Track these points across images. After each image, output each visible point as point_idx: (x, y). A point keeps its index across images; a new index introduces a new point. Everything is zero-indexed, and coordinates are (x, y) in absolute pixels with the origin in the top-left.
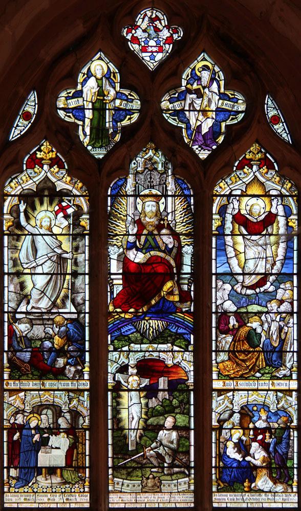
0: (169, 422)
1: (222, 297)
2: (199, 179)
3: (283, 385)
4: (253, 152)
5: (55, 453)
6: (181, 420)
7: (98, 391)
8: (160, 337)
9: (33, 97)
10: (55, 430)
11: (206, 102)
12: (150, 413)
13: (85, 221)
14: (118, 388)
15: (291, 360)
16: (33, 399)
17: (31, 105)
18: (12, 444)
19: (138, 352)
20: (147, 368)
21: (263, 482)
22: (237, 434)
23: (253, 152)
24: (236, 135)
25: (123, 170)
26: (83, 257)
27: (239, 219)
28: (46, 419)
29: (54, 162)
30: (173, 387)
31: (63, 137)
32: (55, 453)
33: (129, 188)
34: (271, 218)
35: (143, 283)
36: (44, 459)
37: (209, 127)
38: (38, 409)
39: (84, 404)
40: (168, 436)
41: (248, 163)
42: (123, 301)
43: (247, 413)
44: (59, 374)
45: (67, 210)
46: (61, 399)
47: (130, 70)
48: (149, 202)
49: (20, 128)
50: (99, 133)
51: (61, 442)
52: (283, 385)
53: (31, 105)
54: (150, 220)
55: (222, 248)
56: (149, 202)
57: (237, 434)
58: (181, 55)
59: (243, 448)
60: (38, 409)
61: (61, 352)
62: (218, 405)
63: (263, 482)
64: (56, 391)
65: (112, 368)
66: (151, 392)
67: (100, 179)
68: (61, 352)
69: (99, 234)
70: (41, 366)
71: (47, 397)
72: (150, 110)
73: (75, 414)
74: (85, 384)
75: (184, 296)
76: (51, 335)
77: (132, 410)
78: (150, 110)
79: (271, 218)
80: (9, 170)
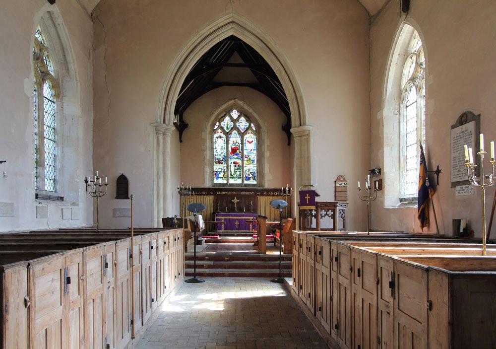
0: (238, 171)
1: (245, 153)
2: (242, 135)
3: (254, 166)
4: (250, 131)
5: (221, 175)
6: (240, 171)
7: (227, 166)
8: (237, 158)
9: (218, 123)
10: (221, 172)
11: (243, 124)
12: (235, 169)
13: (226, 141)
14: (230, 166)
15: (256, 162)
16: (218, 167)
17: (218, 124)
18: (216, 174)
19: (233, 161)
20: (234, 163)
21: (252, 180)
22: (248, 173)
23: (250, 131)
24: (247, 129)
25: (231, 134)
26: (225, 147)
27: (248, 141)
28: (220, 170)
29: (221, 132)
30: (238, 166)
31: (222, 128)
32: (221, 175)
33: (232, 137)
34: (252, 141)
35: (234, 151)
36: (220, 176)
37: (436, 194)
38: (219, 169)
39: (226, 168)
40: (238, 173)
41: (249, 133)
42: (231, 153)
43: (249, 170)
44: (222, 163)
45: (235, 119)
46: (223, 168)
47: (232, 119)
48: (235, 138)
49: (216, 127)
50: (227, 128)
51: (222, 174)
52: (254, 166)
53: (218, 124)
54: (235, 142)
55: (245, 145)
56: (235, 138)
57: (248, 173)
58: (239, 117)
59: (249, 175)
60: (219, 169)
61: (222, 160)
62: (245, 169)
63: (252, 180)
64: (221, 166)
65: (230, 163)
66: (235, 166)
67: (227, 134)
68: (222, 160)
69: (227, 143)
70: (219, 162)
71: (220, 167)
72: (235, 125)
73: (224, 170)
74: (226, 165)
75: (240, 153)
76: (221, 158)
77: (233, 169)
78: (235, 125)
79: (252, 141)
80: (299, 83)
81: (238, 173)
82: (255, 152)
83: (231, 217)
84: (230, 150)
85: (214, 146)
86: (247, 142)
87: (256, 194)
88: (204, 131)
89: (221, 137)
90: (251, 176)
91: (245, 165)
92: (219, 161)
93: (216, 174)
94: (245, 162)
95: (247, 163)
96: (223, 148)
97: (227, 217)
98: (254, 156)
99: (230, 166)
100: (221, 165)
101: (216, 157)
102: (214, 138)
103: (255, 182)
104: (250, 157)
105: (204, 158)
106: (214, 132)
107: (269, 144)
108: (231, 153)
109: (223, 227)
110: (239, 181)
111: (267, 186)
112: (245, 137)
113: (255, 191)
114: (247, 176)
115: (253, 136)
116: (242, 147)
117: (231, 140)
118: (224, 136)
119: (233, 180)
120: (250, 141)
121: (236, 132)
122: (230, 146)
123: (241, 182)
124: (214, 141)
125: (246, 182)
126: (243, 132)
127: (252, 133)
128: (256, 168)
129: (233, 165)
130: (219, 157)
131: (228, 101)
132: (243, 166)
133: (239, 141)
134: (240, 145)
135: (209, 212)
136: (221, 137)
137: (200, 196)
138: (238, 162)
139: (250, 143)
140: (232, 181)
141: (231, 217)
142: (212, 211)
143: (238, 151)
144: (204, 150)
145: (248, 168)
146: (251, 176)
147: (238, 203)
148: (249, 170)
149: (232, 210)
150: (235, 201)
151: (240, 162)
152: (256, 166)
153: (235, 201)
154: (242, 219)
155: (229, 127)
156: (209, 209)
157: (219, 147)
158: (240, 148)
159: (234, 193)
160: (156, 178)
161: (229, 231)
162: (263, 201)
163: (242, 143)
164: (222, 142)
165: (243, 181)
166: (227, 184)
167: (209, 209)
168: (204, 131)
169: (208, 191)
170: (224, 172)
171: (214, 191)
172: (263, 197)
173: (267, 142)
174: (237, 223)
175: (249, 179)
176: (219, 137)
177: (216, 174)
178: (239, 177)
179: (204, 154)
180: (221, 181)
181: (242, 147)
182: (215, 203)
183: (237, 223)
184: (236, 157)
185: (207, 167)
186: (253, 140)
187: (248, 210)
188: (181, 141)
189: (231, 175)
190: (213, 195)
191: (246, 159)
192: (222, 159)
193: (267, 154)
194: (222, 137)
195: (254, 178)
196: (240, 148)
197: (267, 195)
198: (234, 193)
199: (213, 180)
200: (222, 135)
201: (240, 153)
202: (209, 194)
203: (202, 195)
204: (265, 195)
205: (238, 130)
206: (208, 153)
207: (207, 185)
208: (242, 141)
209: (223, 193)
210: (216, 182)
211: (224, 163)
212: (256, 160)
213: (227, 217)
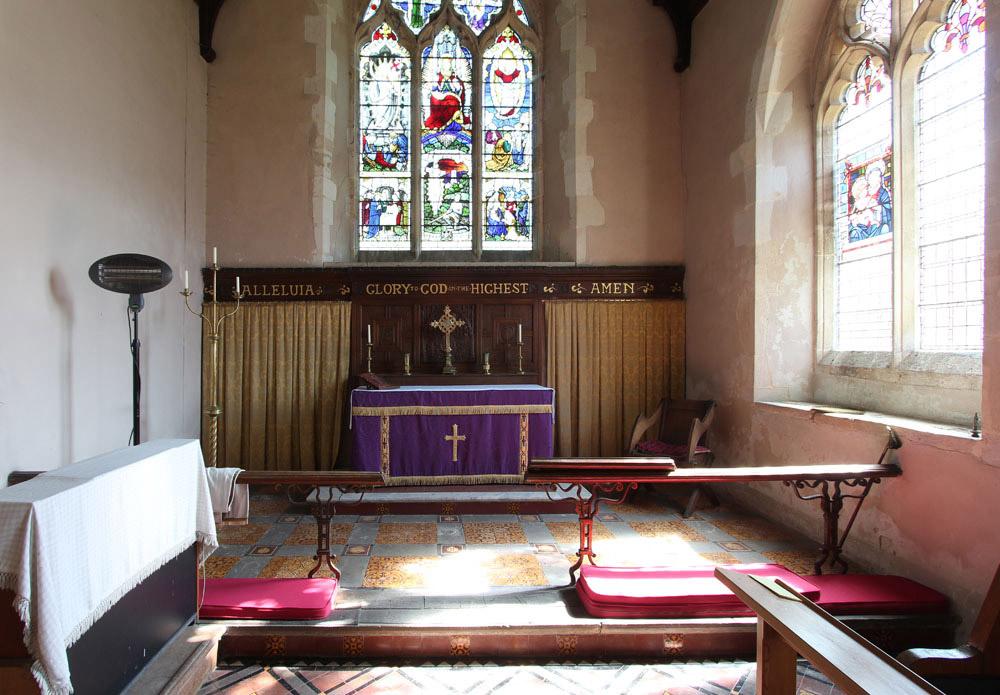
0: (457, 197)
1: (488, 121)
2: (474, 47)
5: (389, 217)
6: (465, 197)
7: (415, 180)
8: (452, 145)
10: (390, 203)
13: (408, 73)
14: (427, 177)
15: (528, 160)
16: (377, 183)
18: (366, 212)
20: (445, 164)
21: (512, 232)
22: (497, 205)
27: (499, 74)
28: (385, 196)
29: (391, 36)
30: (459, 176)
32: (389, 217)
33: (434, 53)
34: (516, 74)
35: (442, 113)
38: (381, 189)
39: (407, 187)
40: (457, 207)
41: (502, 39)
42: (431, 123)
43: (502, 193)
44: (393, 167)
46: (394, 183)
48: (445, 62)
50: (417, 18)
51: (394, 210)
54: (447, 74)
55: (488, 91)
56: (445, 62)
57: (497, 205)
59: (500, 213)
61: (394, 154)
62: (487, 188)
63: (512, 232)
66: (447, 179)
67: (417, 46)
68: (394, 154)
69: (416, 81)
70: (382, 162)
71: (385, 183)
73: (402, 193)
75: (466, 121)
76: (387, 143)
77: (435, 190)
79: (516, 74)
81: (457, 207)
82: (527, 118)
83: (425, 410)
84: (427, 113)
85: (363, 94)
86: (493, 77)
87: (536, 295)
88: (315, 12)
89: (390, 56)
90: (509, 219)
91: (485, 174)
92: (380, 155)
93: (369, 214)
94: (487, 161)
95: (493, 164)
96: (399, 102)
97: (406, 410)
98: (521, 136)
99: (427, 177)
100: (387, 173)
101: (371, 139)
102: (364, 61)
103: (524, 244)
104: (506, 137)
105: (314, 133)
106: (365, 33)
107: (593, 69)
108: (431, 123)
109: (386, 460)
110: (462, 241)
111: (584, 252)
112: (488, 53)
113: (535, 276)
114: (495, 218)
115: (517, 49)
116: (476, 97)
117: (431, 69)
118: (403, 52)
119: (437, 236)
120: (508, 72)
121: (452, 35)
122: (426, 93)
123: (467, 246)
124: (362, 73)
125: (489, 245)
126: (478, 32)
127: (513, 39)
128: (528, 187)
129: (436, 172)
130: (380, 142)
131: (439, 268)
132: (476, 178)
133: (464, 73)
134: (468, 86)
135: (330, 378)
136: (390, 56)
137: (290, 307)
138: (457, 159)
139: (508, 79)
140: (431, 242)
141: (425, 410)
142: (344, 374)
143: (457, 113)
144: (312, 98)
145: (499, 184)
146: (509, 219)
147: (457, 333)
148: (502, 193)
149: (431, 369)
150: (448, 323)
151: (464, 160)
152: (529, 175)
153: (448, 323)
154: (482, 417)
155: (422, 13)
156: (331, 363)
157: (384, 97)
158: (468, 102)
159: (442, 288)
160: (543, 342)
161: (416, 478)
162: (563, 318)
163: (475, 80)
164: (395, 75)
165: (476, 240)
166: (411, 254)
167: (331, 363)
168: (315, 12)
169: (326, 283)
170: (400, 203)
171: (359, 283)
172: (568, 306)
173: (584, 60)
174: (456, 437)
175: (502, 229)
176: (381, 56)
177: (369, 214)
178: (461, 223)
179: (313, 115)
180: (387, 241)
181: (476, 97)
182: (358, 334)
183: (456, 437)
184: (449, 138)
185: (327, 172)
186: (520, 66)
187: (505, 369)
188: (208, 53)
189: (430, 215)
190: (347, 298)
191: (490, 148)
192: (392, 148)
193: (583, 113)
194: (395, 56)
195: (521, 227)
196: (468, 102)
197: (586, 296)
198: (442, 288)
199: (352, 237)
200: (394, 47)
201: (466, 121)
202: (331, 296)
203: (298, 299)
204: (575, 296)
205: (458, 24)
206: (329, 111)
207: (326, 252)
208: (475, 71)
209: (395, 288)
210: (367, 244)
211: (399, 166)
212: (529, 151)
213: (406, 410)
